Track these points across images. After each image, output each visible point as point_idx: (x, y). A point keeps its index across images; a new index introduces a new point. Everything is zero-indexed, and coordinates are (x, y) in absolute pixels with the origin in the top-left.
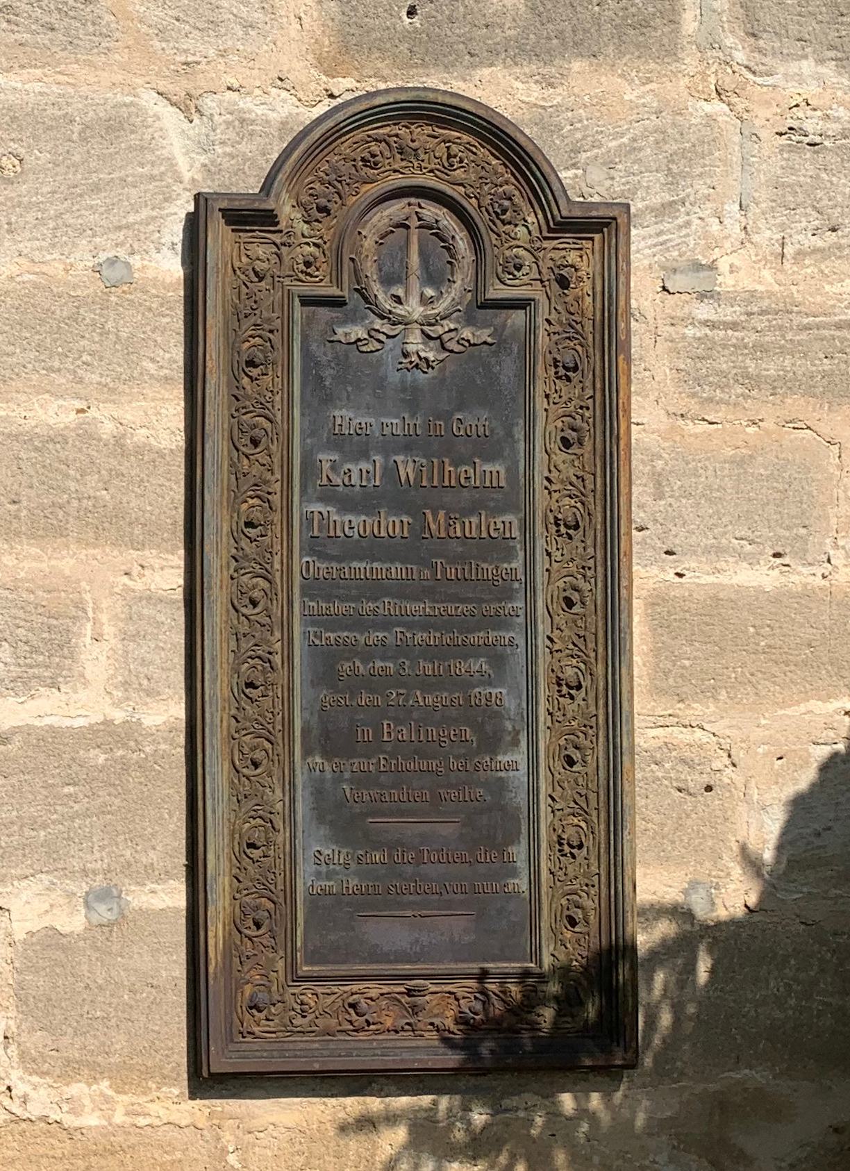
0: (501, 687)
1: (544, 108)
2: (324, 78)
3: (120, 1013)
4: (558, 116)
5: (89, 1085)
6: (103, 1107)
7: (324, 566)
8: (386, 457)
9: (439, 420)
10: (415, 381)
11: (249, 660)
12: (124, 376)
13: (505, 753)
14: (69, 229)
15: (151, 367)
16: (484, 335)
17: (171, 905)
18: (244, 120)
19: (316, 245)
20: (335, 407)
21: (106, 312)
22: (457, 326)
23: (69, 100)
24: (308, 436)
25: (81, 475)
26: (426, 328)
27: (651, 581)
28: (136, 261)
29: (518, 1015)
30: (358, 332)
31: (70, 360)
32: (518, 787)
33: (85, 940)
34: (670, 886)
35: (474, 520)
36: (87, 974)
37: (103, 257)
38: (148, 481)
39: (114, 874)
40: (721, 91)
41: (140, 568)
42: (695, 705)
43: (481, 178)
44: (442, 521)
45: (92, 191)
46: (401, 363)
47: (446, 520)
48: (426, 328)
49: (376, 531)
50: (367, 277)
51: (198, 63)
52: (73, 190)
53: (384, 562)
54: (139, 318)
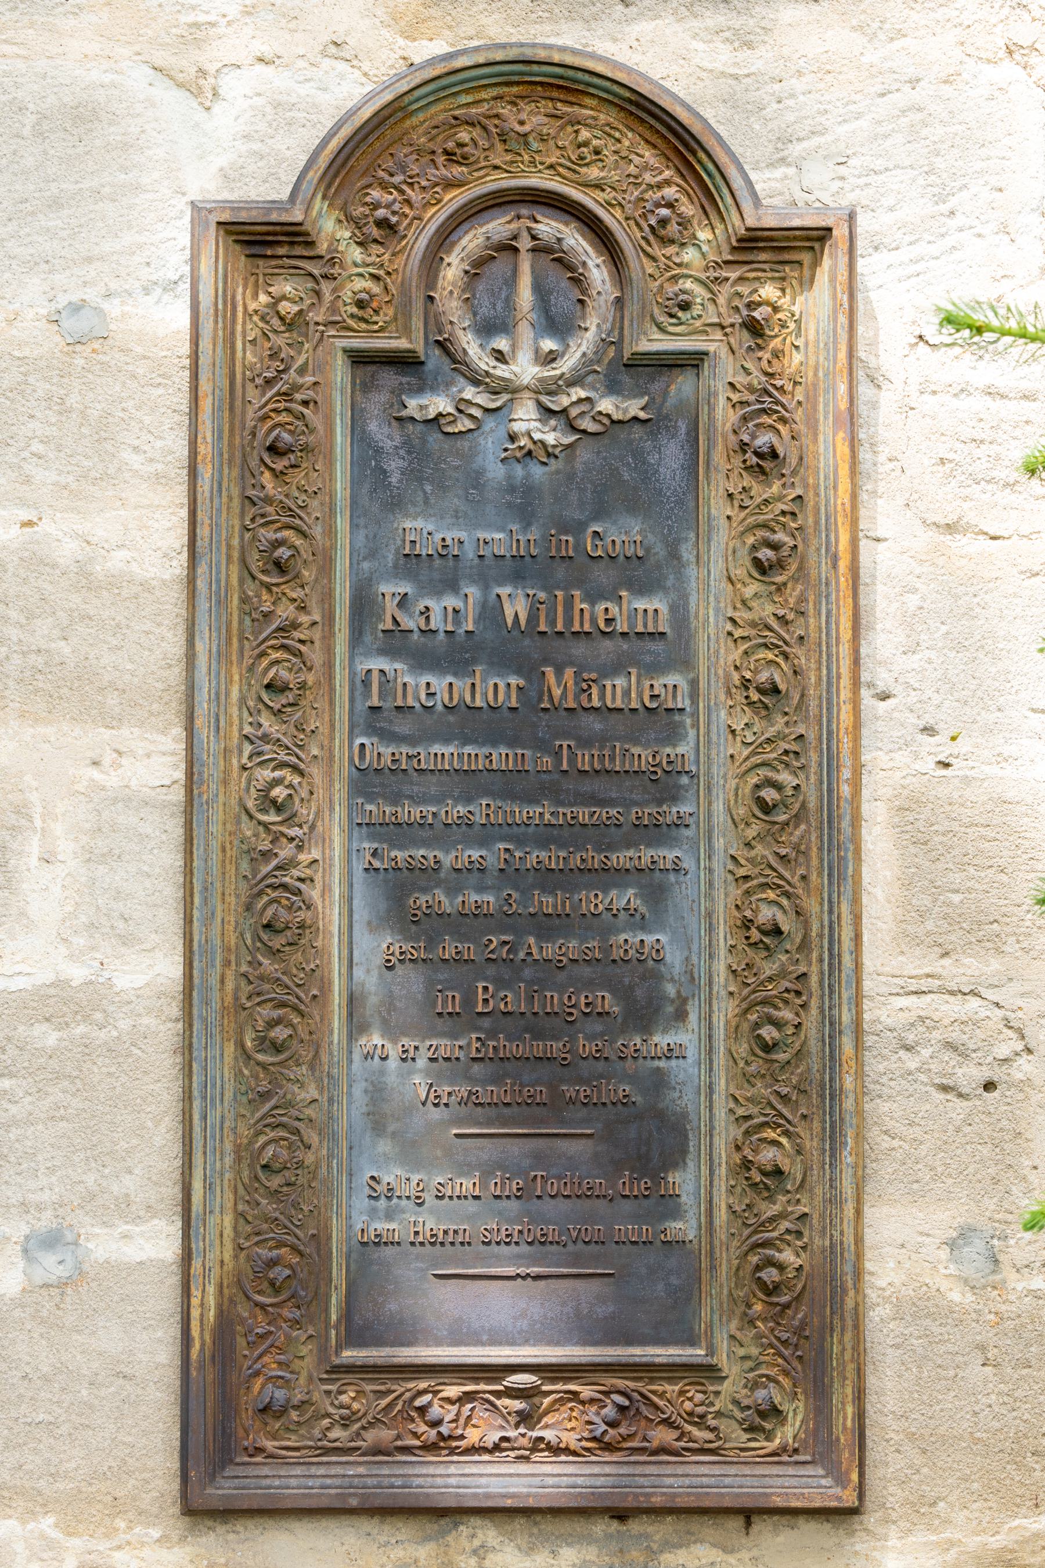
0: (656, 931)
1: (736, 77)
2: (401, 42)
3: (74, 1416)
4: (758, 89)
5: (24, 1522)
6: (45, 1556)
7: (390, 750)
8: (486, 588)
9: (566, 533)
10: (528, 476)
11: (269, 891)
12: (93, 474)
13: (665, 1031)
14: (14, 262)
15: (135, 461)
16: (634, 407)
17: (153, 1255)
18: (279, 104)
19: (376, 278)
20: (407, 515)
21: (66, 380)
22: (591, 394)
23: (19, 80)
24: (365, 559)
25: (28, 618)
26: (544, 399)
27: (898, 774)
28: (113, 308)
29: (677, 1428)
30: (440, 404)
31: (14, 450)
32: (684, 1083)
33: (23, 1307)
34: (928, 1235)
35: (620, 682)
36: (27, 1358)
37: (62, 301)
38: (128, 627)
39: (68, 1208)
40: (1013, 48)
41: (115, 755)
42: (967, 961)
43: (629, 176)
44: (571, 683)
45: (50, 206)
46: (506, 450)
47: (576, 683)
48: (544, 399)
49: (468, 699)
50: (451, 322)
51: (213, 25)
52: (22, 206)
53: (483, 744)
54: (118, 388)
